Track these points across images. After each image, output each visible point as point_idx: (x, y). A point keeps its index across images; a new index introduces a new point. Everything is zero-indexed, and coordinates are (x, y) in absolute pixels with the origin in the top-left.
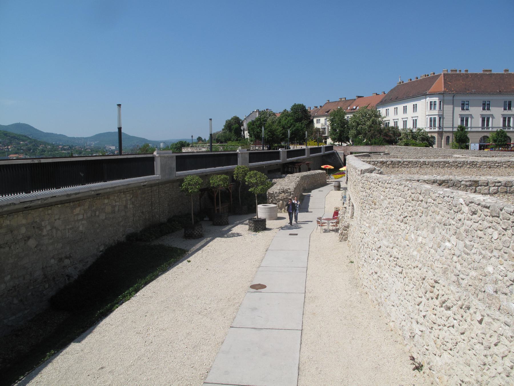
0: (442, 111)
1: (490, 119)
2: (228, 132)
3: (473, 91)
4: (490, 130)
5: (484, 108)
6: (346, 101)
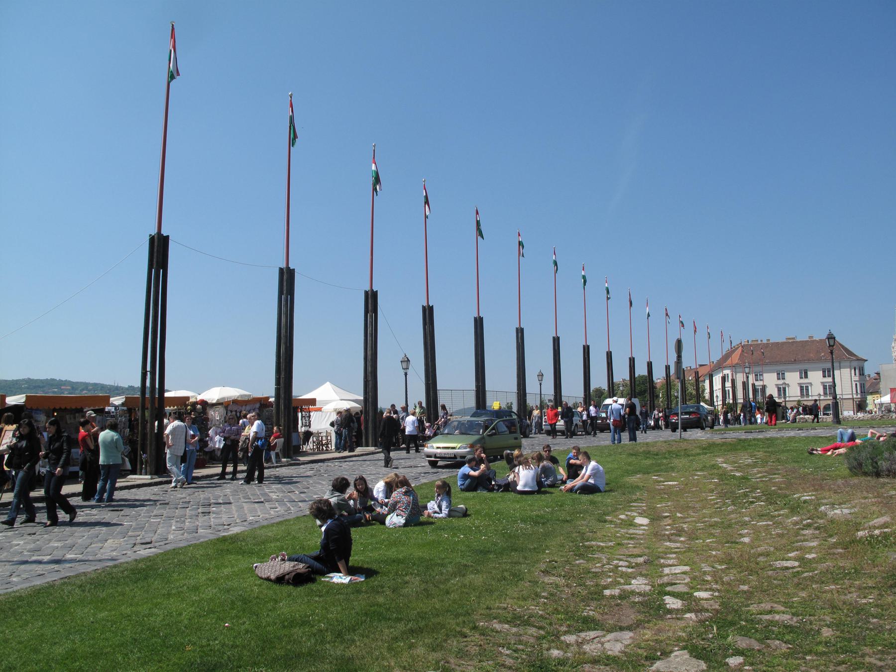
4: (810, 398)
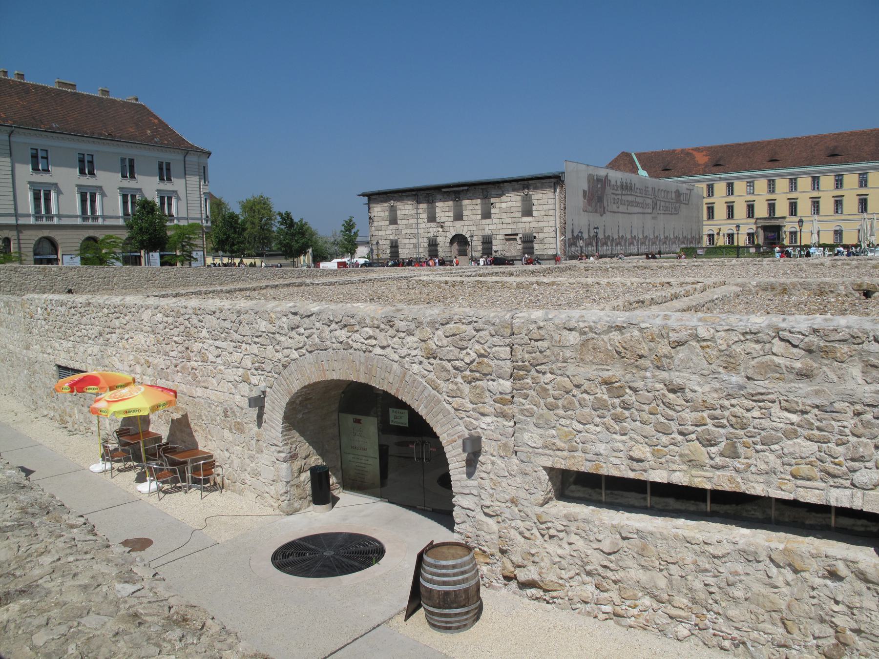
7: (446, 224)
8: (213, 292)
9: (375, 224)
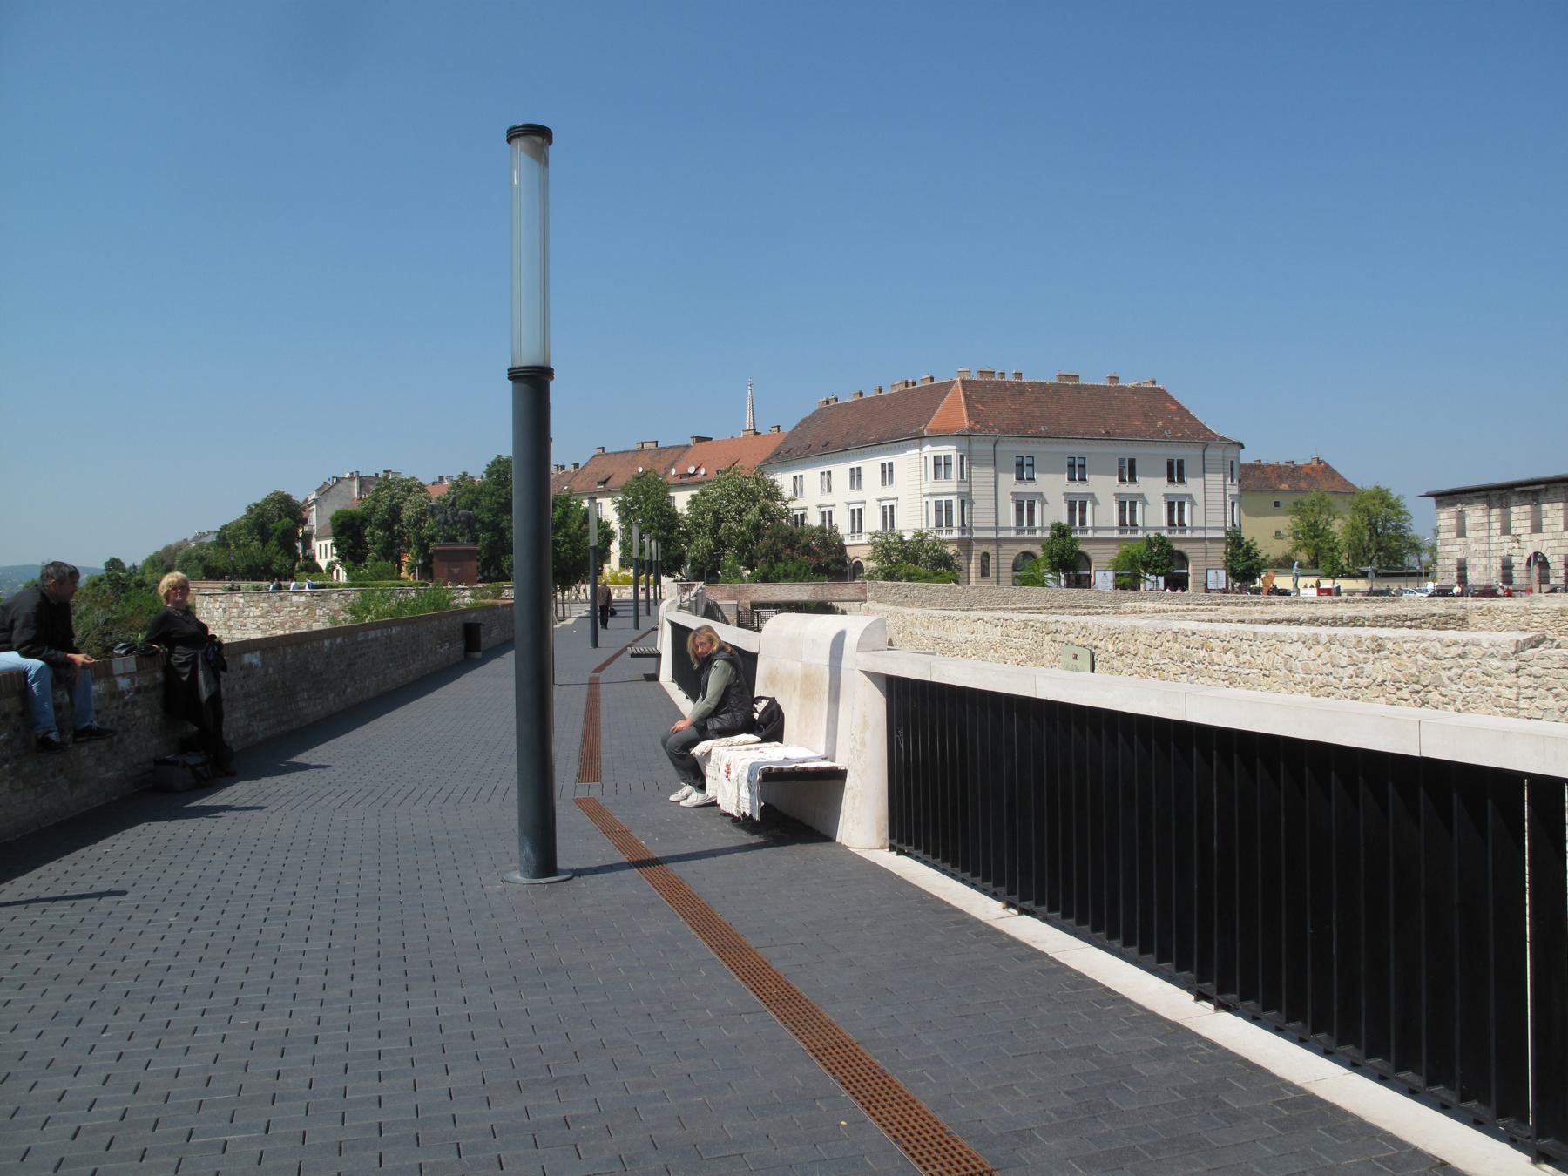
0: (967, 484)
1: (1089, 506)
2: (255, 543)
3: (1043, 429)
5: (1083, 477)
6: (660, 451)
7: (1523, 538)
8: (1000, 609)
9: (1441, 536)
